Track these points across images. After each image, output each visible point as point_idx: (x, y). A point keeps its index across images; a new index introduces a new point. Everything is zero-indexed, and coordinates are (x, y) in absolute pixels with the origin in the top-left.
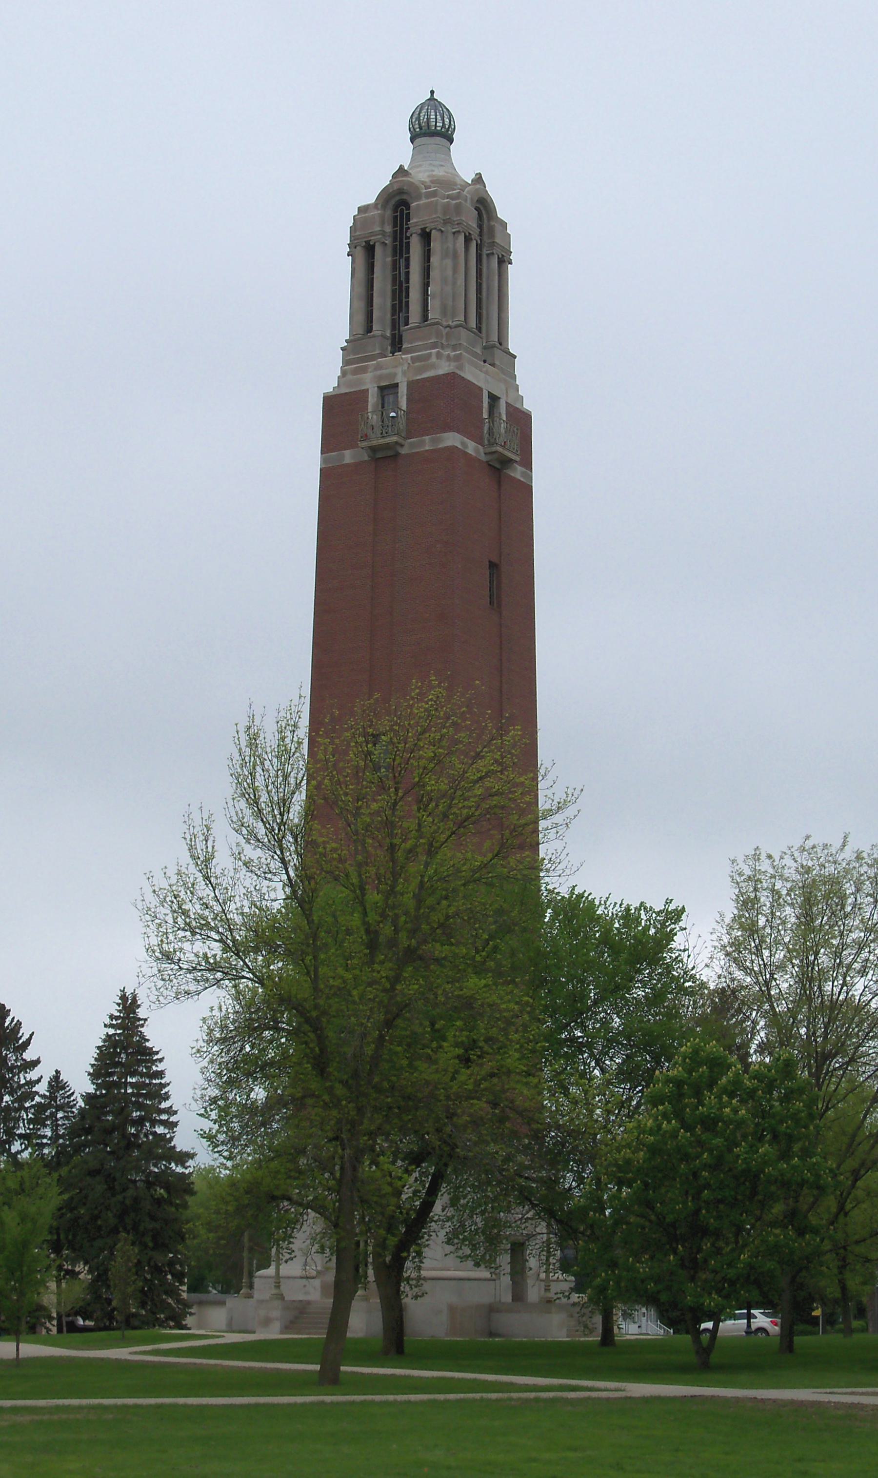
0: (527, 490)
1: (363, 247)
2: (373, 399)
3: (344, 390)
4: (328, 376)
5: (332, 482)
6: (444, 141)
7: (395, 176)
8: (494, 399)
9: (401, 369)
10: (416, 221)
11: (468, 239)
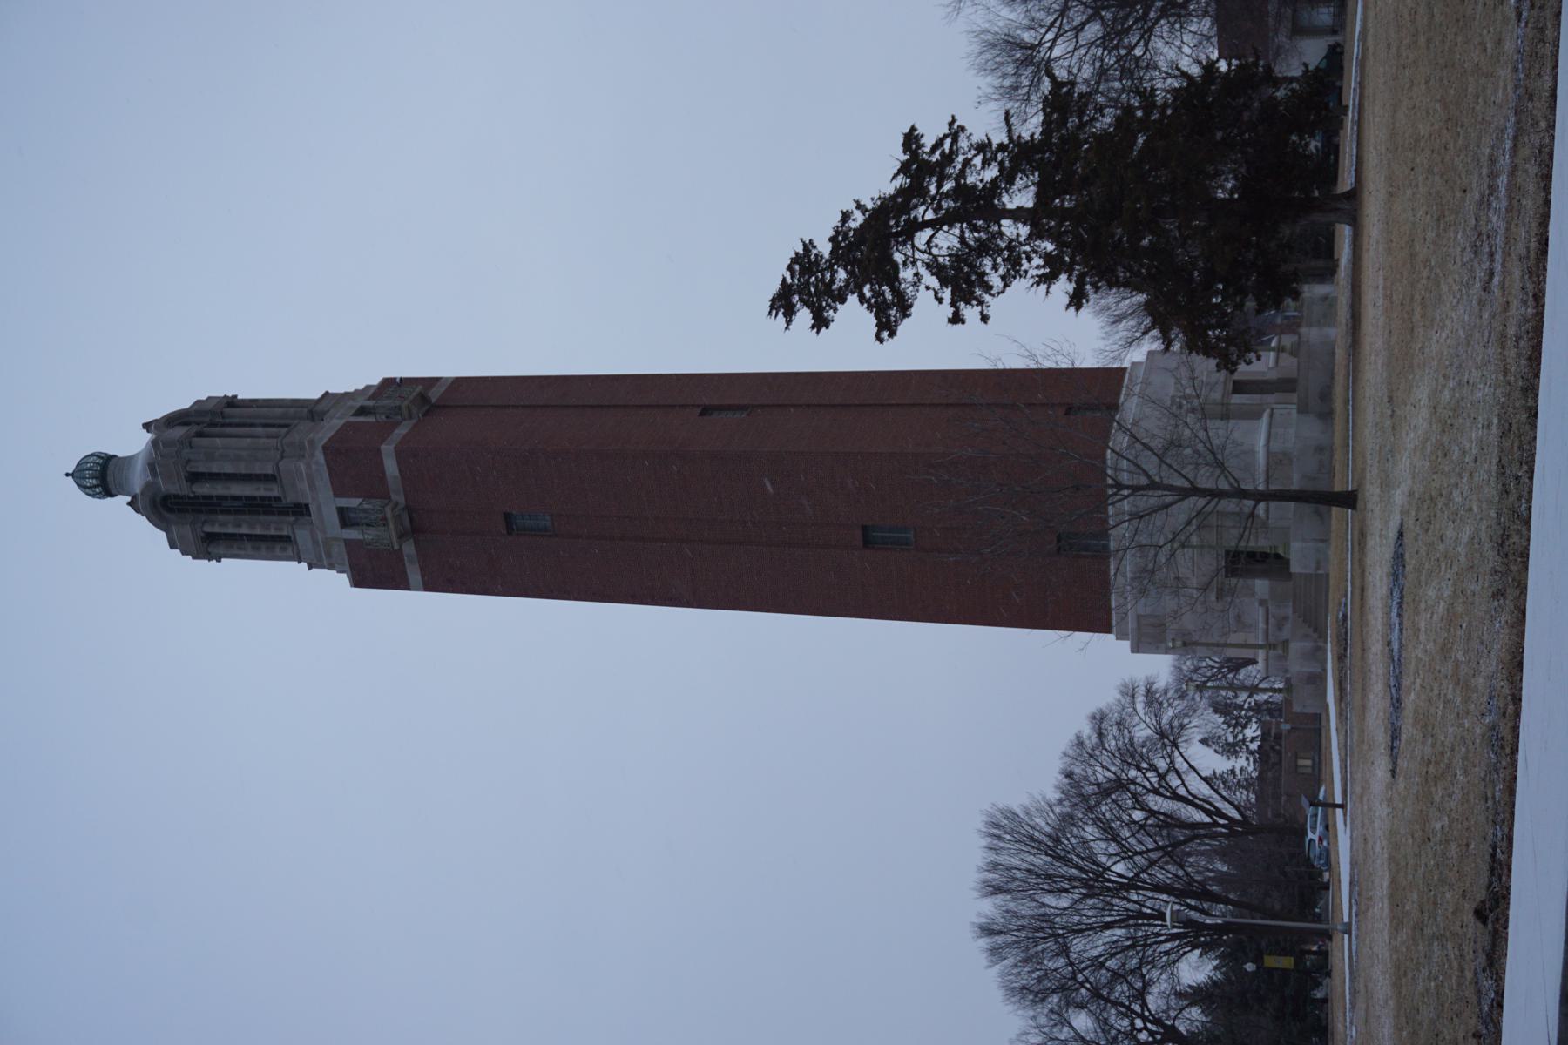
0: (459, 382)
1: (207, 546)
2: (353, 534)
3: (347, 567)
4: (335, 582)
5: (438, 581)
6: (112, 461)
7: (137, 511)
8: (362, 411)
9: (326, 505)
10: (179, 488)
11: (200, 435)
